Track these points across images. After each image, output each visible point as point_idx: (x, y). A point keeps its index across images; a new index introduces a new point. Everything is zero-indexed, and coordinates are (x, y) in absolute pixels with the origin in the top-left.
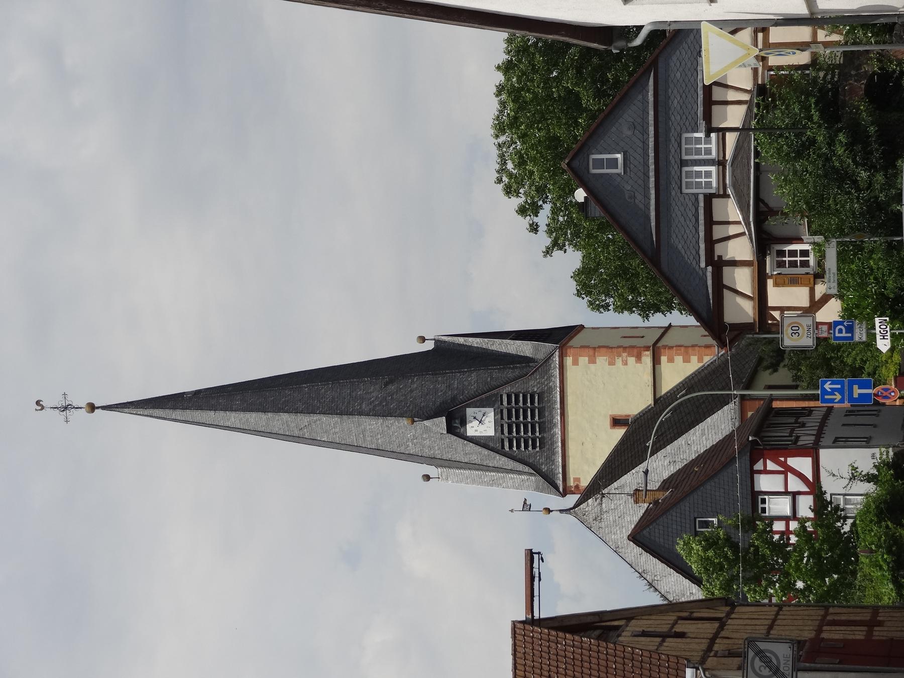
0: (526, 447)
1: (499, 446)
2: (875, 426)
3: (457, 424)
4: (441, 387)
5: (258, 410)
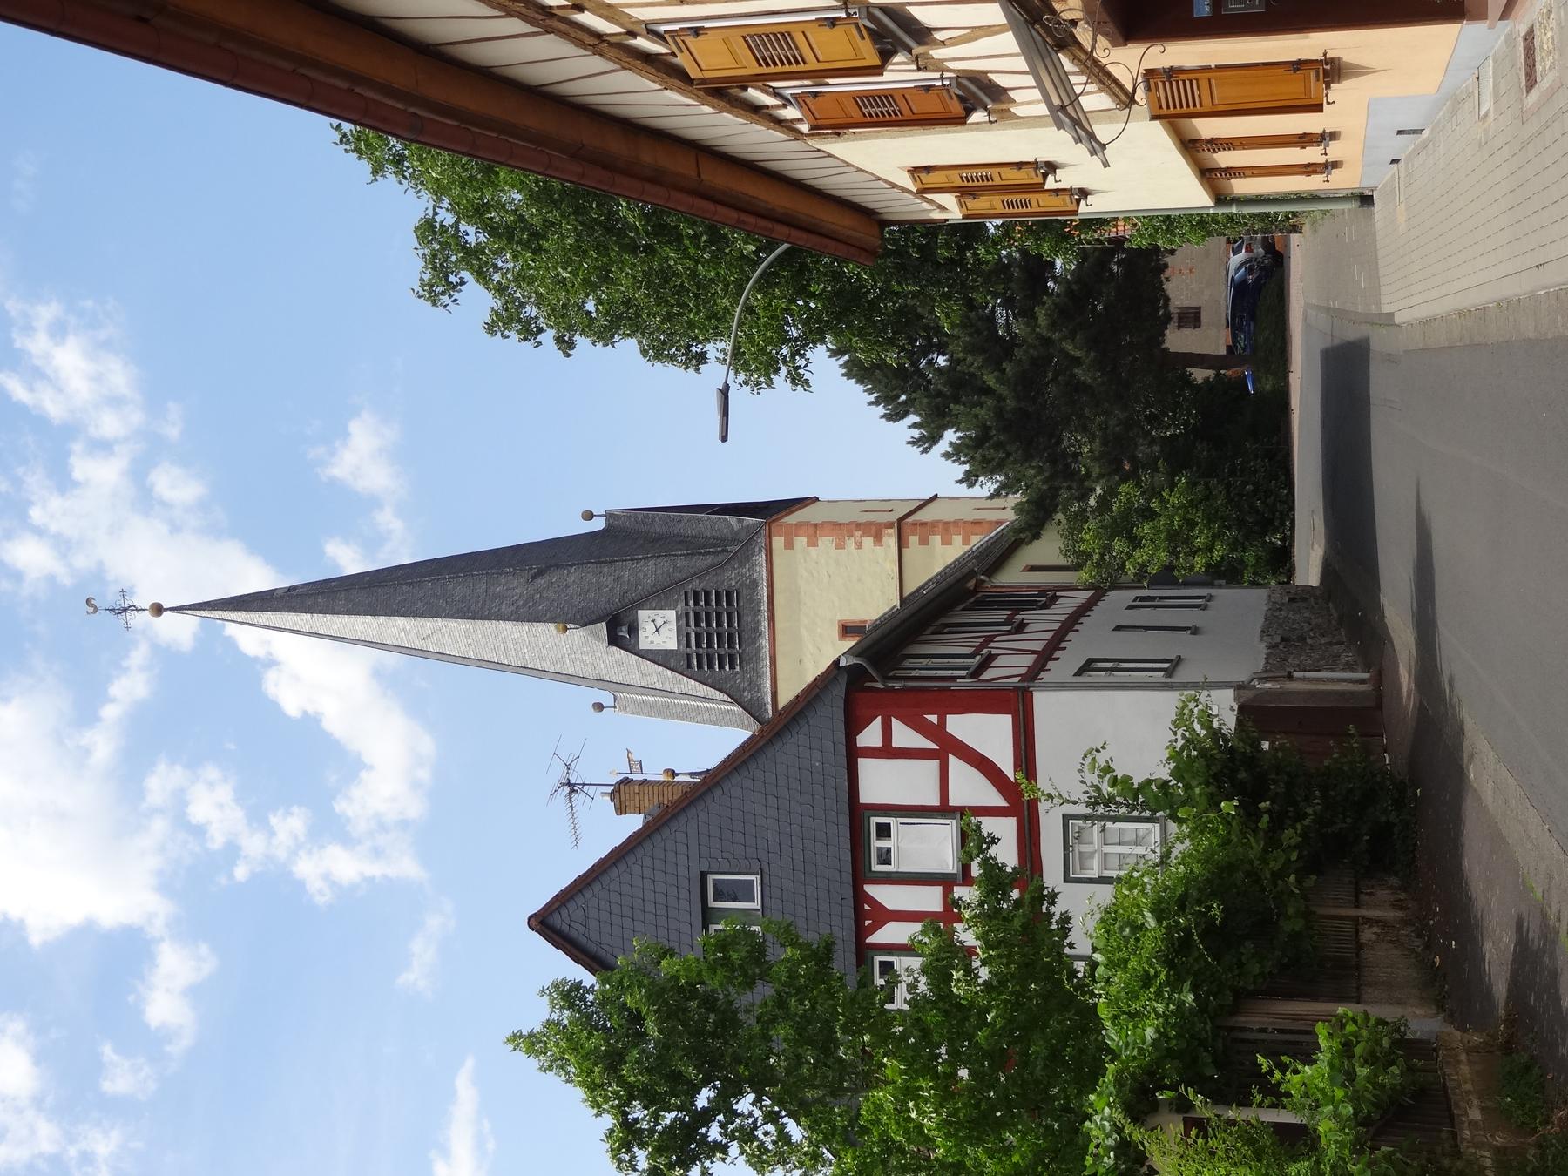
0: (721, 667)
2: (1195, 631)
3: (624, 632)
4: (606, 583)
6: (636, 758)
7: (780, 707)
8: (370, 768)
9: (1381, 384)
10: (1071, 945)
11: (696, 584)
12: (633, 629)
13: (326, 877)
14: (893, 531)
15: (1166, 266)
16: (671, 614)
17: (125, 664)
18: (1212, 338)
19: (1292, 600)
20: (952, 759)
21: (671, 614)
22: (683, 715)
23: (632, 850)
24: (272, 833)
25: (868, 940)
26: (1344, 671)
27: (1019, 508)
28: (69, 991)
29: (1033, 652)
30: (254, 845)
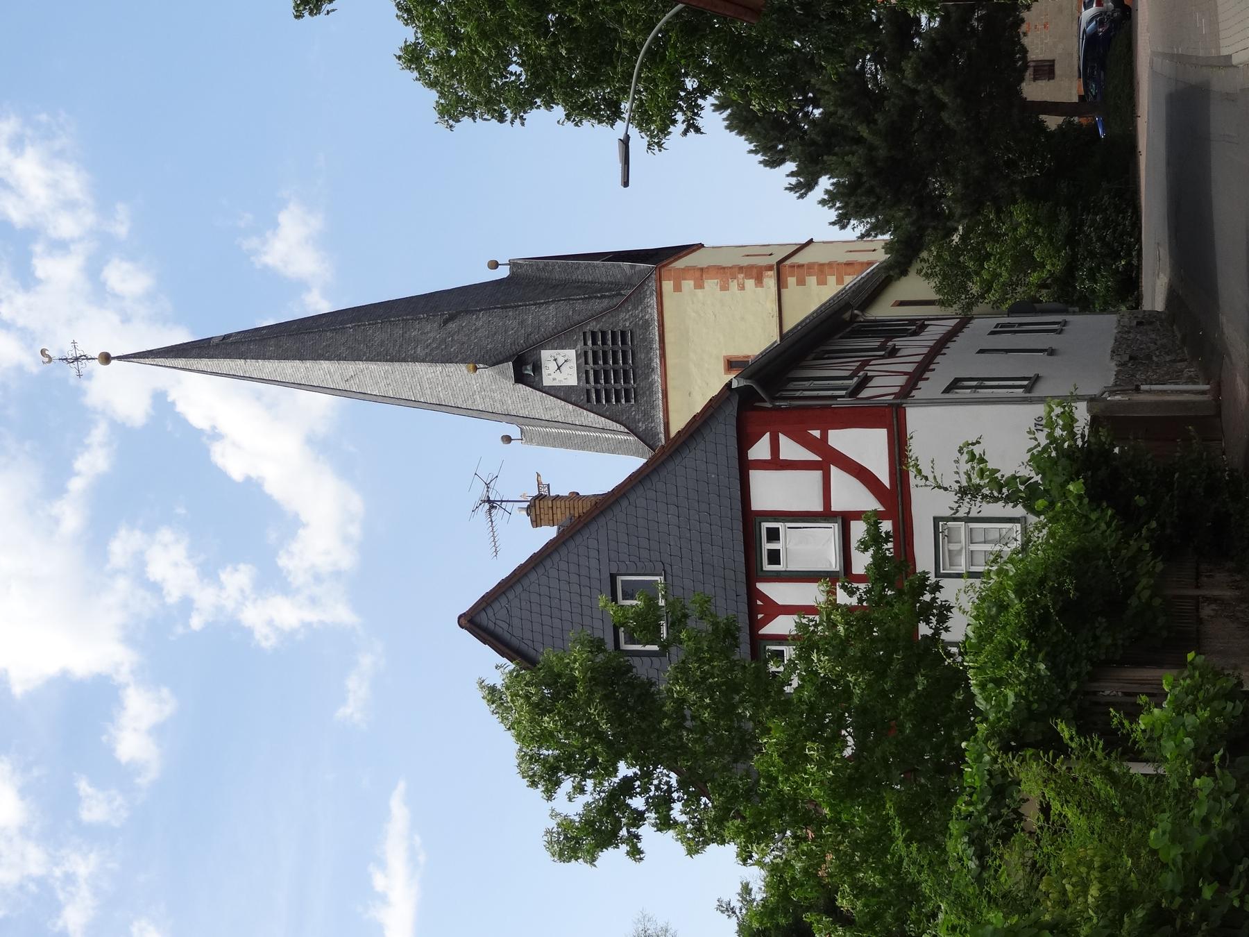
1: (584, 397)
2: (1052, 352)
3: (529, 371)
4: (511, 326)
6: (544, 481)
7: (673, 433)
8: (305, 526)
9: (1221, 121)
12: (537, 368)
13: (270, 623)
15: (1023, 21)
16: (571, 354)
17: (87, 441)
18: (1066, 88)
19: (1140, 324)
20: (834, 471)
21: (571, 354)
22: (584, 445)
23: (549, 555)
24: (221, 587)
25: (761, 632)
26: (1186, 383)
27: (888, 247)
28: (59, 730)
29: (905, 373)
30: (205, 597)
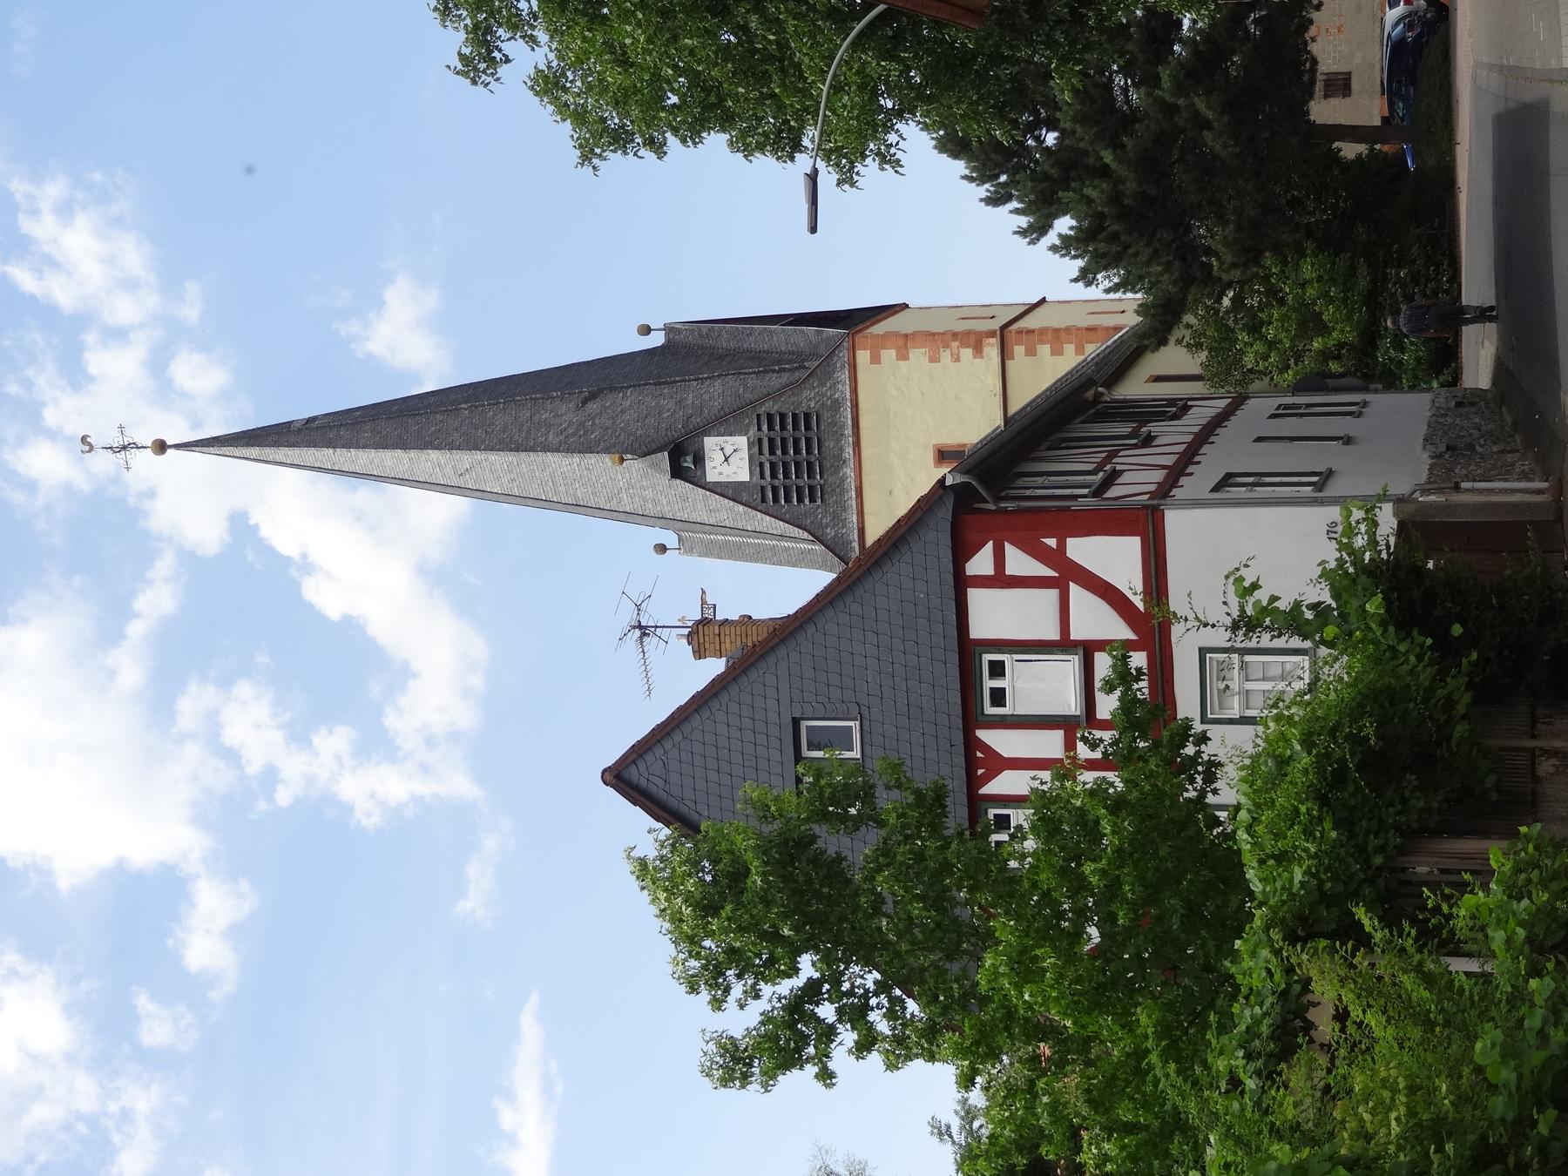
0: (800, 500)
2: (1348, 440)
3: (688, 463)
5: (395, 446)
10: (1215, 792)
11: (770, 407)
12: (699, 459)
14: (994, 341)
15: (1311, 22)
16: (742, 441)
18: (1365, 107)
19: (1459, 405)
21: (742, 441)
22: (757, 556)
25: (982, 791)
26: (1519, 480)
27: (1142, 310)
29: (1163, 467)
